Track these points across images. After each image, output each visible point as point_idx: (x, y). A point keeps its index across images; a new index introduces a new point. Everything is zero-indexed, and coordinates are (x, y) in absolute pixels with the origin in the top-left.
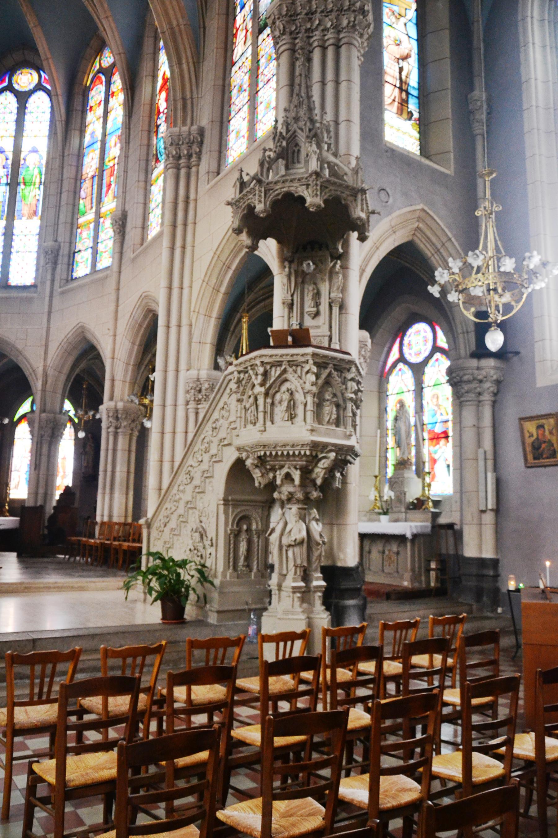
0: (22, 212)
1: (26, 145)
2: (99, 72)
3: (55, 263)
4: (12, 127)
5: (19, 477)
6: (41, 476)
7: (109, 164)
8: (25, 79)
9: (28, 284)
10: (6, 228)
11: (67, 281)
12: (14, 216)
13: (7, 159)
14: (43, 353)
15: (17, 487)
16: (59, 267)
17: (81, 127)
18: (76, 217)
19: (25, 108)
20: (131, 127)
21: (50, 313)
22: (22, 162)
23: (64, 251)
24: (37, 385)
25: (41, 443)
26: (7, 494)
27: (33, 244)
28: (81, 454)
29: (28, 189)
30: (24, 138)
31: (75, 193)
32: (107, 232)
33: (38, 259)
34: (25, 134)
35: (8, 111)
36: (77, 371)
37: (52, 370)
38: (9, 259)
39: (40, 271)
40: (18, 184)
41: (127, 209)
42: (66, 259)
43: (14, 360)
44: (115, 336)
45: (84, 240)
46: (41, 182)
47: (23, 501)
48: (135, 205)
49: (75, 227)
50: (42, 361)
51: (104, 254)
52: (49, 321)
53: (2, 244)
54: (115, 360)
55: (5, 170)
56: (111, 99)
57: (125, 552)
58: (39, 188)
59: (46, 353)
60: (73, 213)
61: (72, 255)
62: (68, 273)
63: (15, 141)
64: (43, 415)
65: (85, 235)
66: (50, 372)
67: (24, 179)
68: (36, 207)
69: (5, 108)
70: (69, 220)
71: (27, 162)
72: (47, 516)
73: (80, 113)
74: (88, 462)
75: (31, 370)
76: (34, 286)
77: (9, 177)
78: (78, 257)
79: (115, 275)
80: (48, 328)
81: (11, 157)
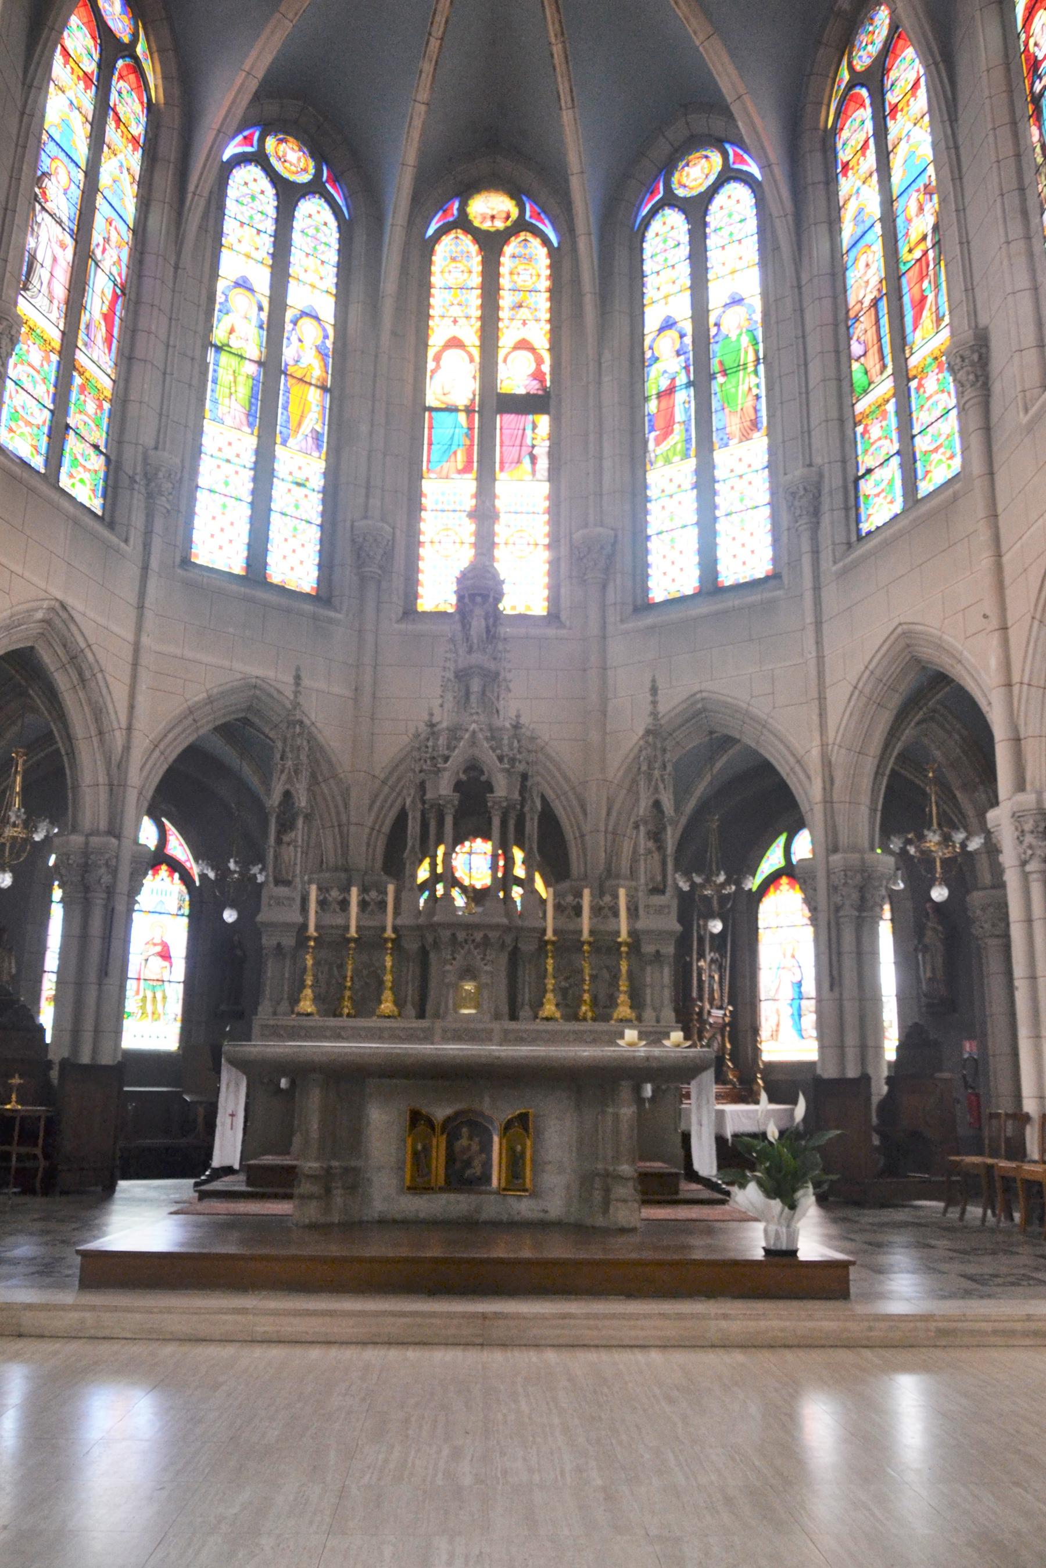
0: (728, 430)
1: (717, 295)
2: (851, 86)
3: (816, 513)
4: (684, 270)
5: (778, 1011)
6: (848, 1005)
7: (907, 257)
8: (696, 173)
9: (760, 574)
10: (697, 472)
11: (849, 545)
12: (712, 443)
13: (682, 336)
14: (815, 718)
15: (774, 1035)
16: (826, 520)
17: (829, 215)
18: (847, 402)
19: (705, 225)
20: (960, 140)
21: (818, 624)
22: (713, 331)
23: (833, 480)
24: (810, 792)
25: (838, 924)
26: (757, 1052)
27: (758, 489)
28: (916, 950)
29: (732, 379)
30: (710, 284)
31: (837, 352)
32: (938, 399)
33: (774, 518)
34: (711, 275)
35: (671, 243)
36: (899, 747)
37: (843, 751)
38: (714, 533)
39: (785, 538)
40: (712, 377)
41: (983, 320)
42: (839, 498)
43: (753, 745)
44: (1004, 628)
45: (877, 444)
46: (758, 359)
47: (812, 1065)
48: (1010, 298)
49: (849, 424)
50: (816, 735)
51: (935, 457)
52: (819, 643)
53: (695, 505)
54: (1016, 689)
55: (682, 358)
56: (890, 124)
57: (23, 1118)
58: (756, 372)
59: (822, 714)
60: (840, 396)
61: (851, 487)
62: (848, 525)
63: (693, 296)
64: (836, 858)
65: (875, 431)
66: (839, 757)
67: (721, 363)
68: (756, 411)
69: (665, 241)
70: (834, 414)
71: (724, 329)
72: (875, 1100)
73: (821, 186)
74: (933, 969)
75: (792, 760)
76: (773, 577)
77: (692, 368)
78: (866, 487)
79: (979, 486)
80: (820, 658)
81: (688, 327)
